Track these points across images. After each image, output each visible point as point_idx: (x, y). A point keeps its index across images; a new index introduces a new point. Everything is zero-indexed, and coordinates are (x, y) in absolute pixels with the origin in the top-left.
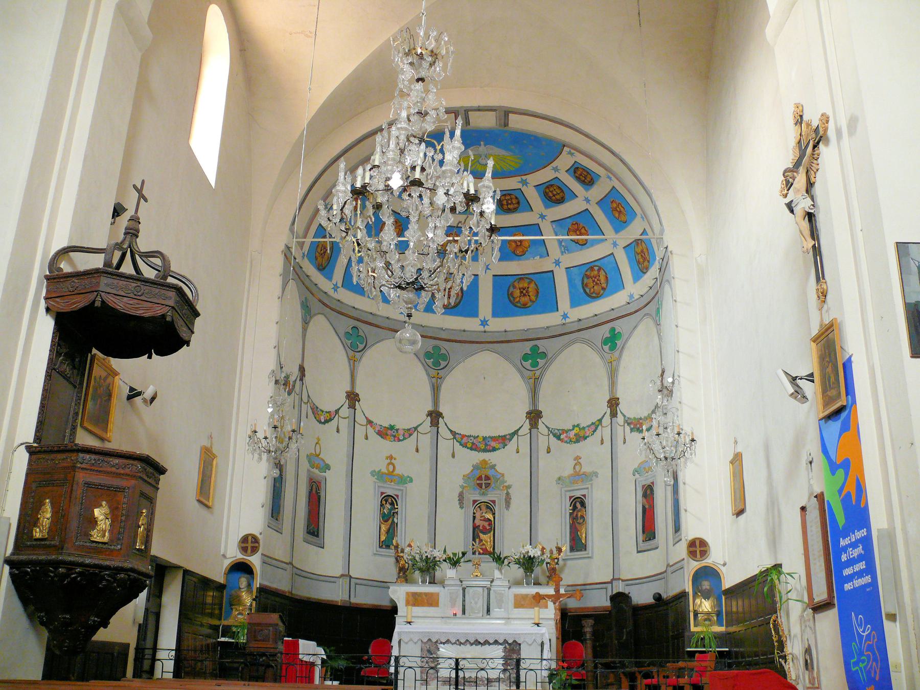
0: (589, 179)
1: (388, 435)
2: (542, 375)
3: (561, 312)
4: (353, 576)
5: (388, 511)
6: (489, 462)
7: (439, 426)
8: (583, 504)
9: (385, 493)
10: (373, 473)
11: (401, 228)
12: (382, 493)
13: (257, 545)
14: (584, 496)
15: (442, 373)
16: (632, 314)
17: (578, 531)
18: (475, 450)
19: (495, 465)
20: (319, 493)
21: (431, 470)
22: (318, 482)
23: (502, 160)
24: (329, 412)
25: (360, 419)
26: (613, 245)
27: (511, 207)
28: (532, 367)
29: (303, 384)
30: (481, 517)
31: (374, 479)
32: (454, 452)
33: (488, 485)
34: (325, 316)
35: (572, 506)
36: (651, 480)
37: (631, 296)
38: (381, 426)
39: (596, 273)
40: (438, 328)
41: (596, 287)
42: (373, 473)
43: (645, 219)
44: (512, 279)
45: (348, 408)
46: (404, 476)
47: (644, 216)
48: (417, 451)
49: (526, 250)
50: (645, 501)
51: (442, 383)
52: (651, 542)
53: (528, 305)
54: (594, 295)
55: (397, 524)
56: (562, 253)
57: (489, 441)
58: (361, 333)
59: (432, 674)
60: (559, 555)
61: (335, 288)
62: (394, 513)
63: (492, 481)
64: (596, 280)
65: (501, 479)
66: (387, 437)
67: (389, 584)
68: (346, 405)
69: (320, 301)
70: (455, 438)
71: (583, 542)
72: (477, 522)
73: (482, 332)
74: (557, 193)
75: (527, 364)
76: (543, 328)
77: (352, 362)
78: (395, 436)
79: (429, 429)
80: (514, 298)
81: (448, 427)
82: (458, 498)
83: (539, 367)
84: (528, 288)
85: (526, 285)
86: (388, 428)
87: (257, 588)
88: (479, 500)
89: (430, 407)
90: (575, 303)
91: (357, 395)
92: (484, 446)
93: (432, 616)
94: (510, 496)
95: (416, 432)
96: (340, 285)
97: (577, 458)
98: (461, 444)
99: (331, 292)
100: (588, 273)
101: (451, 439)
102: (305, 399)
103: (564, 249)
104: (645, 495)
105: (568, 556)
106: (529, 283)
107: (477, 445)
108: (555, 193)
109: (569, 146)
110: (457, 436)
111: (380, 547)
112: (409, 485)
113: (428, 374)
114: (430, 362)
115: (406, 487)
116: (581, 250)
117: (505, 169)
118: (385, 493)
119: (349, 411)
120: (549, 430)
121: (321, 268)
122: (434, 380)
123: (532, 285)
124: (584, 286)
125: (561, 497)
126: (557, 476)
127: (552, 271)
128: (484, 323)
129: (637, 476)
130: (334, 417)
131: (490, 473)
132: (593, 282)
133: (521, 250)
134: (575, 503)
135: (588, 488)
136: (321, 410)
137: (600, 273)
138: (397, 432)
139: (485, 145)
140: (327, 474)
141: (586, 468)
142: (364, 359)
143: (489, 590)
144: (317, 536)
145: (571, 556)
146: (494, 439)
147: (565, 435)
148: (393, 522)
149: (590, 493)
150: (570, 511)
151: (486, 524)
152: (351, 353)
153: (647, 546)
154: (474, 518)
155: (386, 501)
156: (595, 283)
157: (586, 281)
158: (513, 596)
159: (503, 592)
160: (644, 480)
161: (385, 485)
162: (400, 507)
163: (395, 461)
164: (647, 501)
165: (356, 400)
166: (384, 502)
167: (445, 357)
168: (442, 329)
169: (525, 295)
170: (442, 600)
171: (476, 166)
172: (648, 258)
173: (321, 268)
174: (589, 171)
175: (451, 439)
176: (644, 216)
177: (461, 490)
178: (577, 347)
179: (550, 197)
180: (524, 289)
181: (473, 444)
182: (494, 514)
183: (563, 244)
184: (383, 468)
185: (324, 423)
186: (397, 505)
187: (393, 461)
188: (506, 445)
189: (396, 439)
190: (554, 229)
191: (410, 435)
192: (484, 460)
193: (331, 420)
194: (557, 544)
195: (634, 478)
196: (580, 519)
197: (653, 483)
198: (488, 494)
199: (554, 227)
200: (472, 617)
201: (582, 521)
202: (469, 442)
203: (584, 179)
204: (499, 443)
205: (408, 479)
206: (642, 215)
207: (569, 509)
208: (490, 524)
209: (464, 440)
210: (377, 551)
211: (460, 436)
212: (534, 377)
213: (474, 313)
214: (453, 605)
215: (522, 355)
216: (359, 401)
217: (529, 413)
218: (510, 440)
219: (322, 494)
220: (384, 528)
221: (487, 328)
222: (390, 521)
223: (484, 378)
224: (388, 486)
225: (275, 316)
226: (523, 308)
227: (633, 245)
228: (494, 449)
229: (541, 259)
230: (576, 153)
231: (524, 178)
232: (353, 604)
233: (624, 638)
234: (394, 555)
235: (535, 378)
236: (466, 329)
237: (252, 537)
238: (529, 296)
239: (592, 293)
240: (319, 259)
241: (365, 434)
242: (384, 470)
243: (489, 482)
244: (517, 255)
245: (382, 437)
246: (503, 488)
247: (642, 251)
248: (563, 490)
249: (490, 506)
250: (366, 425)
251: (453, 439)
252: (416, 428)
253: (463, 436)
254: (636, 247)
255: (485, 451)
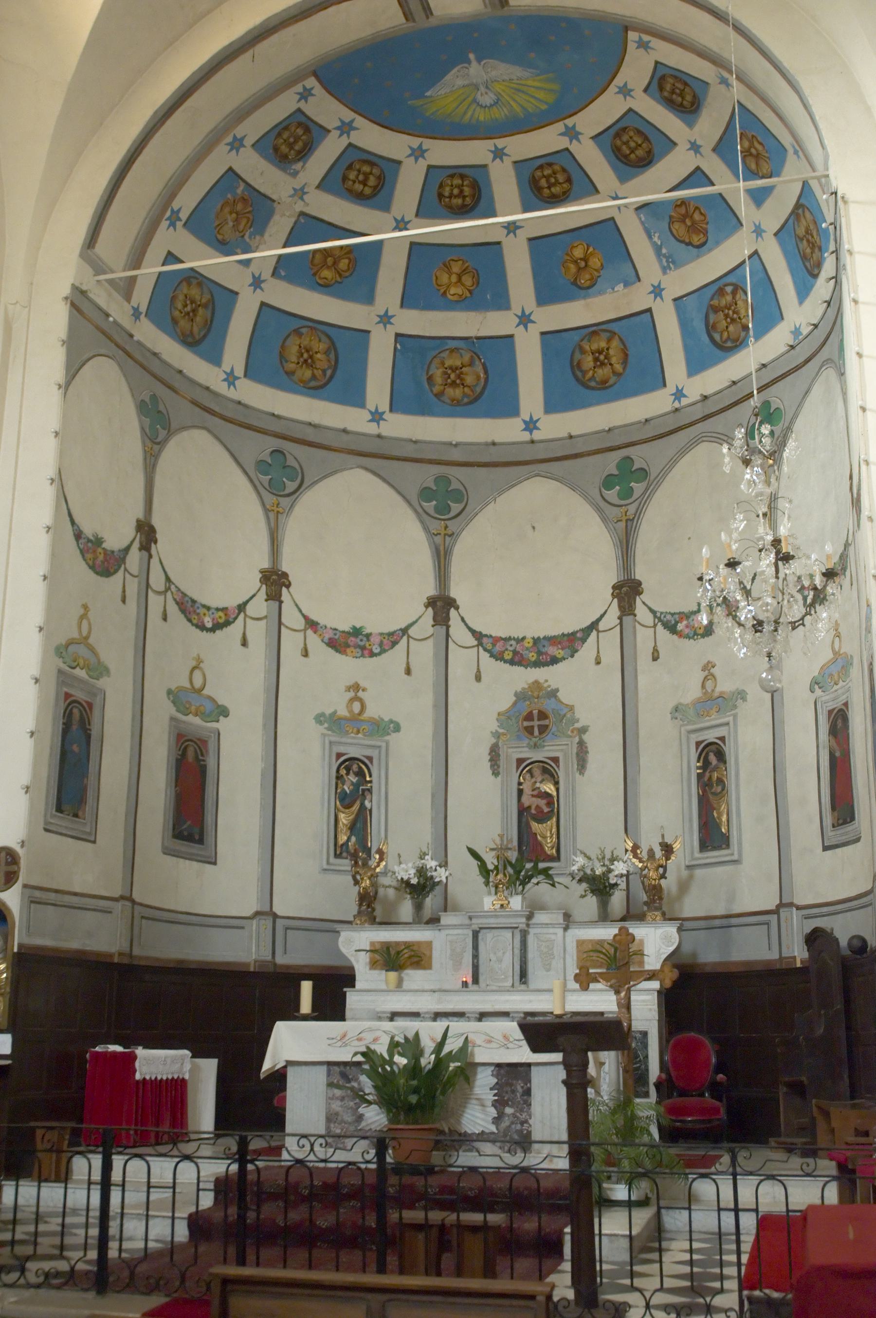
0: (689, 98)
1: (349, 646)
2: (639, 512)
3: (671, 388)
4: (279, 913)
5: (351, 787)
6: (546, 685)
7: (451, 623)
8: (721, 756)
9: (344, 754)
10: (320, 719)
11: (351, 256)
12: (339, 755)
13: (15, 868)
14: (722, 739)
15: (453, 526)
16: (801, 368)
17: (714, 809)
18: (519, 664)
19: (557, 690)
20: (204, 761)
21: (435, 706)
22: (199, 739)
23: (519, 90)
24: (224, 610)
25: (291, 617)
26: (755, 234)
27: (556, 190)
28: (621, 499)
29: (150, 556)
30: (533, 790)
31: (322, 729)
32: (478, 671)
33: (543, 729)
34: (209, 431)
35: (701, 761)
36: (843, 699)
37: (796, 332)
38: (336, 629)
39: (729, 298)
40: (445, 443)
41: (731, 328)
42: (320, 719)
43: (800, 153)
44: (576, 337)
45: (266, 600)
46: (382, 720)
47: (798, 148)
48: (408, 672)
49: (596, 274)
50: (833, 741)
51: (454, 544)
52: (849, 828)
53: (611, 382)
54: (729, 344)
55: (371, 811)
56: (665, 270)
57: (544, 646)
58: (291, 462)
59: (350, 1123)
60: (668, 859)
61: (231, 379)
62: (363, 790)
63: (551, 721)
64: (731, 312)
65: (568, 716)
66: (348, 650)
67: (338, 927)
68: (262, 595)
69: (195, 403)
70: (480, 644)
71: (723, 830)
72: (526, 800)
73: (527, 442)
74: (637, 143)
75: (612, 495)
76: (640, 422)
77: (272, 515)
78: (363, 648)
79: (431, 630)
80: (581, 371)
81: (466, 625)
82: (489, 757)
83: (635, 496)
84: (608, 349)
85: (603, 344)
86: (348, 633)
87: (14, 953)
88: (528, 759)
89: (431, 590)
90: (696, 365)
91: (285, 575)
92: (535, 655)
93: (420, 988)
94: (586, 747)
95: (405, 638)
96: (239, 371)
97: (708, 667)
98: (492, 656)
99: (222, 388)
100: (715, 302)
101: (473, 647)
102: (157, 580)
103: (667, 261)
104: (834, 731)
105: (694, 859)
106: (609, 340)
107: (522, 655)
108: (632, 144)
109: (635, 29)
110: (485, 640)
111: (336, 856)
112: (393, 738)
113: (426, 529)
114: (430, 506)
115: (387, 743)
116: (698, 257)
117: (530, 110)
118: (344, 754)
119: (267, 607)
120: (655, 617)
121: (190, 341)
122: (438, 540)
123: (615, 343)
124: (710, 329)
125: (681, 745)
126: (671, 705)
127: (649, 310)
128: (531, 425)
129: (818, 692)
130: (236, 618)
131: (548, 705)
132: (726, 319)
133: (587, 276)
134: (707, 754)
135: (728, 724)
136: (204, 606)
137: (738, 297)
138: (368, 640)
139: (479, 60)
140: (223, 725)
141: (725, 685)
142: (297, 509)
143: (524, 934)
144: (201, 841)
145: (703, 858)
146: (553, 640)
147: (685, 622)
148: (362, 806)
149: (732, 734)
150: (698, 771)
151: (542, 803)
152: (270, 499)
153: (842, 835)
154: (520, 792)
155: (348, 769)
156: (729, 320)
157: (712, 318)
158: (575, 944)
159: (553, 937)
160: (830, 700)
161: (344, 740)
162: (376, 776)
163: (365, 693)
164: (838, 743)
165: (284, 584)
166: (343, 772)
167: (459, 496)
168: (450, 444)
169: (602, 364)
170: (439, 955)
171: (474, 110)
172: (818, 241)
173: (190, 340)
174: (684, 78)
175: (473, 647)
176: (798, 148)
177: (494, 741)
178: (703, 448)
179: (626, 156)
180: (600, 352)
181: (515, 653)
182: (556, 783)
183: (664, 251)
184: (339, 705)
185: (213, 630)
186: (370, 776)
187: (361, 694)
188: (577, 651)
189: (366, 652)
190: (642, 223)
191: (394, 644)
192: (536, 682)
193: (227, 623)
194: (663, 836)
195: (813, 697)
196: (717, 785)
197: (846, 704)
198: (544, 746)
199: (643, 219)
200: (494, 988)
201: (719, 789)
202: (507, 650)
203: (680, 99)
204: (562, 649)
205: (392, 725)
206: (794, 147)
207: (695, 765)
208: (550, 804)
209: (499, 647)
210: (328, 863)
211: (491, 640)
212: (624, 518)
213: (510, 409)
214: (457, 964)
215: (603, 478)
216: (288, 586)
217: (617, 587)
218: (584, 640)
219: (211, 763)
220: (345, 819)
221: (537, 435)
222: (356, 807)
223: (534, 528)
224: (349, 741)
225: (54, 424)
226: (599, 389)
227: (791, 221)
228: (554, 661)
229: (626, 291)
230: (655, 43)
231: (570, 122)
232: (282, 966)
233: (714, 1060)
234: (349, 868)
235: (627, 520)
236: (497, 440)
237: (8, 854)
238: (611, 364)
239: (725, 342)
240: (183, 323)
241: (302, 645)
242: (343, 712)
243: (546, 722)
244: (580, 288)
245: (337, 651)
246: (572, 732)
247: (808, 231)
248: (683, 729)
249: (549, 770)
250: (305, 630)
251: (478, 646)
252: (405, 631)
253: (496, 640)
254: (796, 227)
255: (537, 664)
